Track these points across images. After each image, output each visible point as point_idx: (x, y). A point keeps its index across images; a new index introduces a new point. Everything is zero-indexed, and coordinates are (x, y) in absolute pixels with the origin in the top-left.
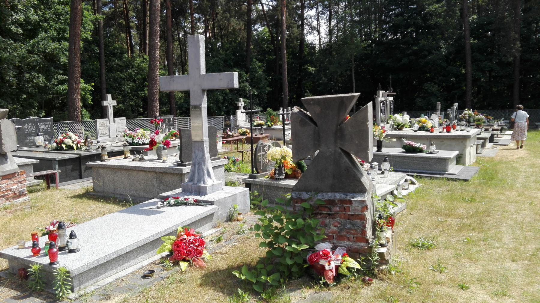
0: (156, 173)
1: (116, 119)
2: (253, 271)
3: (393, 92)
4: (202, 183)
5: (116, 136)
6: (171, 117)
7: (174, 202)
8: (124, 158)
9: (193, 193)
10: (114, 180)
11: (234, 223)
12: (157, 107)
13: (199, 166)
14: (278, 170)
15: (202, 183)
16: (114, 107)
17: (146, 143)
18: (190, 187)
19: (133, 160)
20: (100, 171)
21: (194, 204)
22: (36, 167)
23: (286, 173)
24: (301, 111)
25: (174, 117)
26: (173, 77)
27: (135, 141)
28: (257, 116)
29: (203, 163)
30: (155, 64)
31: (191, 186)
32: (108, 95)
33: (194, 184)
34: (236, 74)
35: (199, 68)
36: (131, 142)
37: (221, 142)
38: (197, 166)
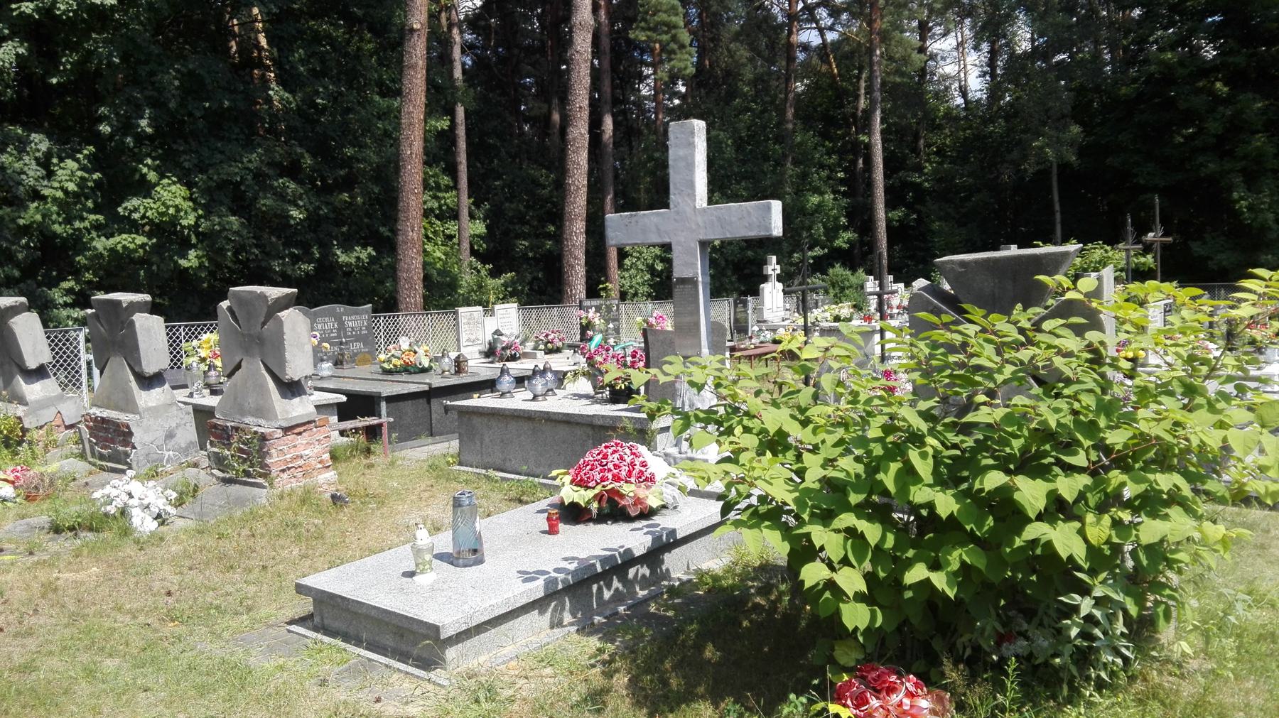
0: (592, 426)
2: (1272, 559)
3: (1162, 236)
20: (474, 422)
22: (345, 412)
24: (1156, 271)
34: (776, 206)
35: (692, 195)
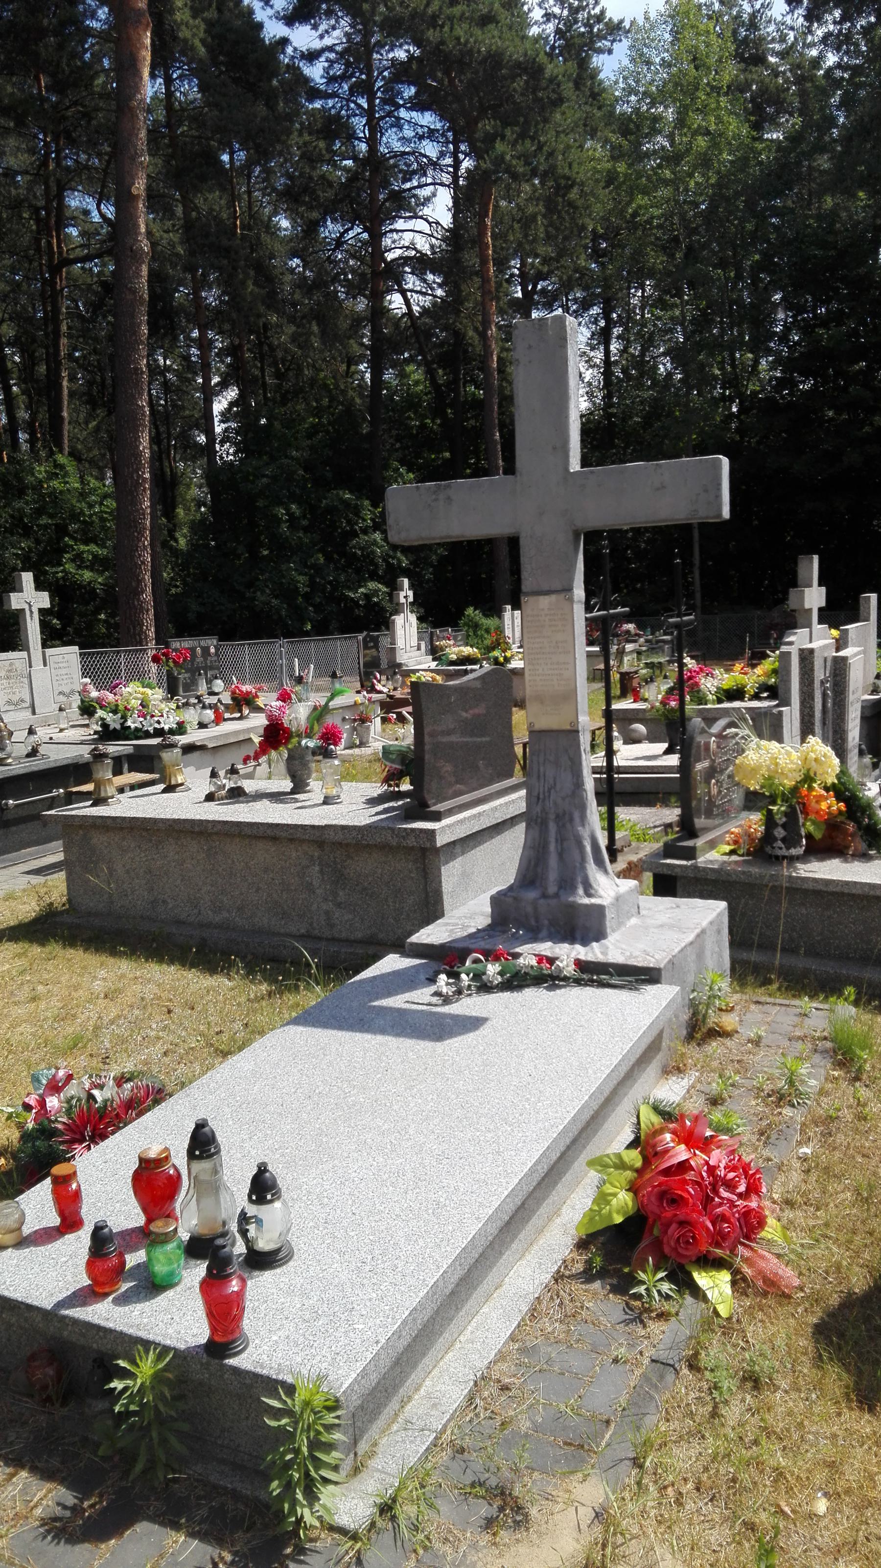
0: (320, 844)
1: (49, 651)
4: (581, 891)
5: (61, 710)
6: (209, 642)
7: (501, 973)
8: (164, 791)
9: (544, 933)
10: (149, 871)
11: (714, 1046)
12: (148, 610)
13: (561, 828)
14: (784, 826)
15: (581, 891)
16: (41, 611)
17: (166, 727)
18: (529, 909)
19: (210, 798)
20: (94, 841)
21: (578, 982)
23: (809, 836)
25: (220, 640)
26: (449, 486)
27: (129, 723)
28: (445, 634)
29: (576, 815)
30: (139, 476)
31: (534, 903)
32: (24, 574)
33: (544, 896)
36: (118, 727)
37: (378, 720)
38: (552, 827)
